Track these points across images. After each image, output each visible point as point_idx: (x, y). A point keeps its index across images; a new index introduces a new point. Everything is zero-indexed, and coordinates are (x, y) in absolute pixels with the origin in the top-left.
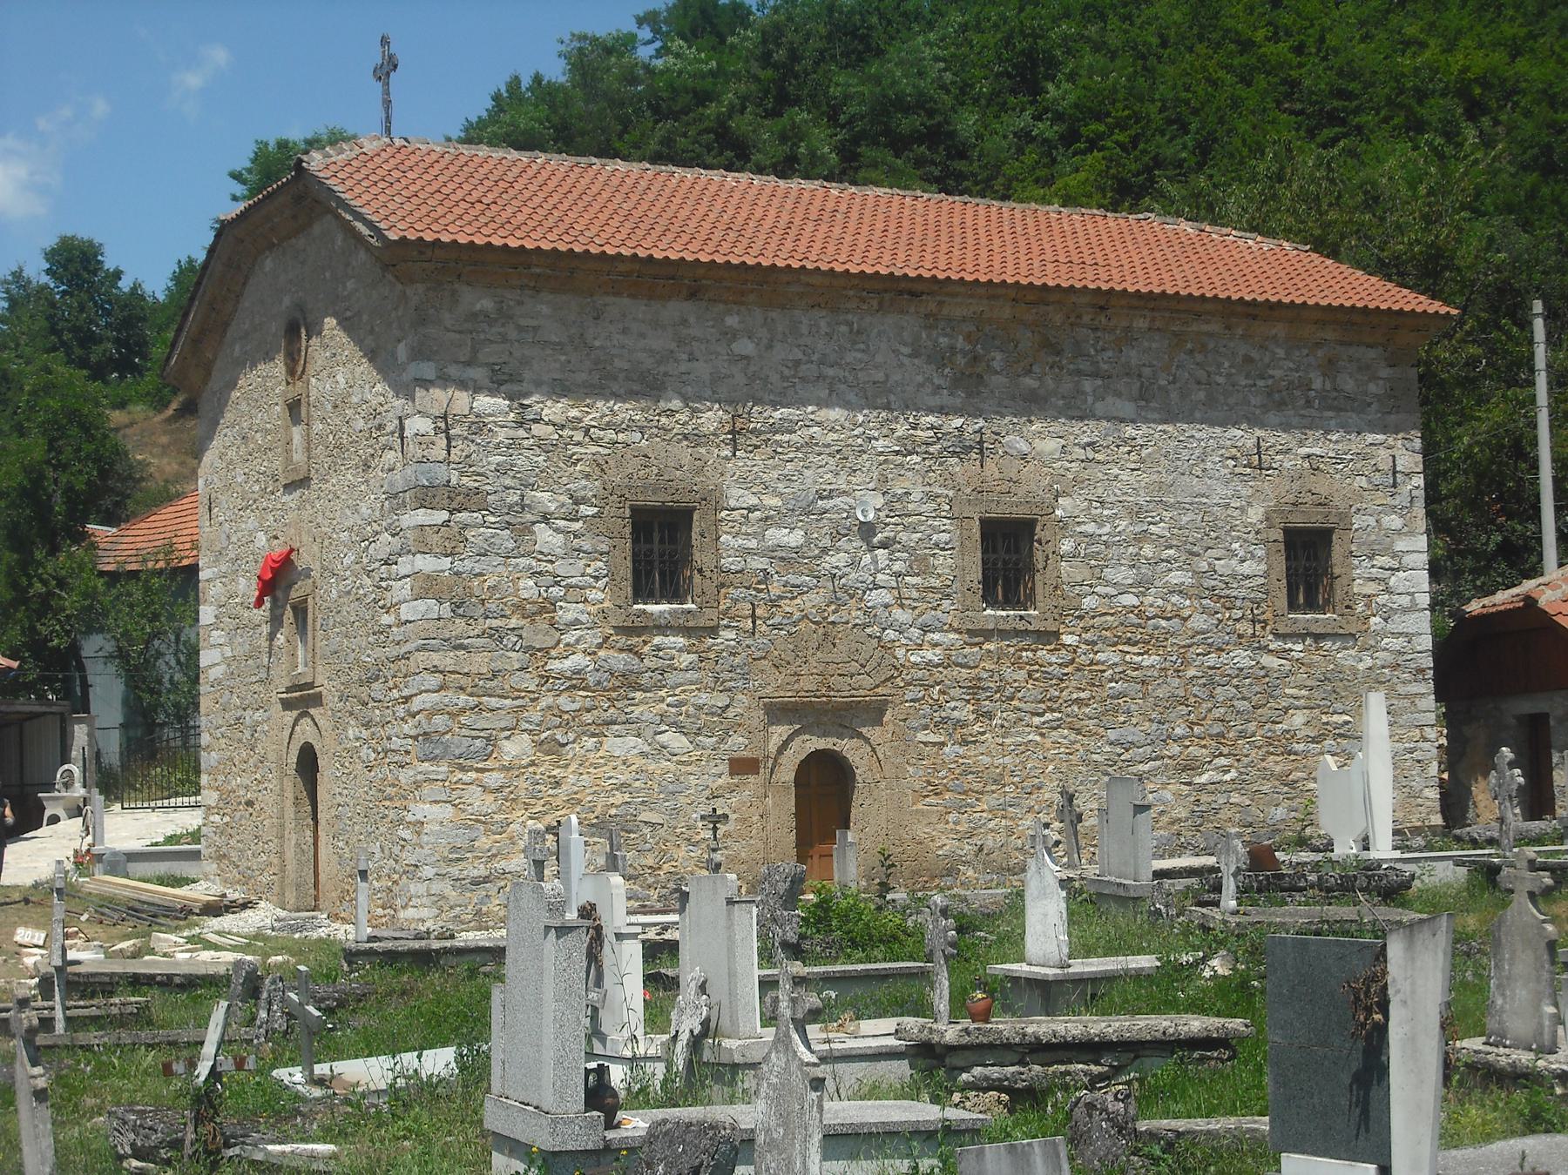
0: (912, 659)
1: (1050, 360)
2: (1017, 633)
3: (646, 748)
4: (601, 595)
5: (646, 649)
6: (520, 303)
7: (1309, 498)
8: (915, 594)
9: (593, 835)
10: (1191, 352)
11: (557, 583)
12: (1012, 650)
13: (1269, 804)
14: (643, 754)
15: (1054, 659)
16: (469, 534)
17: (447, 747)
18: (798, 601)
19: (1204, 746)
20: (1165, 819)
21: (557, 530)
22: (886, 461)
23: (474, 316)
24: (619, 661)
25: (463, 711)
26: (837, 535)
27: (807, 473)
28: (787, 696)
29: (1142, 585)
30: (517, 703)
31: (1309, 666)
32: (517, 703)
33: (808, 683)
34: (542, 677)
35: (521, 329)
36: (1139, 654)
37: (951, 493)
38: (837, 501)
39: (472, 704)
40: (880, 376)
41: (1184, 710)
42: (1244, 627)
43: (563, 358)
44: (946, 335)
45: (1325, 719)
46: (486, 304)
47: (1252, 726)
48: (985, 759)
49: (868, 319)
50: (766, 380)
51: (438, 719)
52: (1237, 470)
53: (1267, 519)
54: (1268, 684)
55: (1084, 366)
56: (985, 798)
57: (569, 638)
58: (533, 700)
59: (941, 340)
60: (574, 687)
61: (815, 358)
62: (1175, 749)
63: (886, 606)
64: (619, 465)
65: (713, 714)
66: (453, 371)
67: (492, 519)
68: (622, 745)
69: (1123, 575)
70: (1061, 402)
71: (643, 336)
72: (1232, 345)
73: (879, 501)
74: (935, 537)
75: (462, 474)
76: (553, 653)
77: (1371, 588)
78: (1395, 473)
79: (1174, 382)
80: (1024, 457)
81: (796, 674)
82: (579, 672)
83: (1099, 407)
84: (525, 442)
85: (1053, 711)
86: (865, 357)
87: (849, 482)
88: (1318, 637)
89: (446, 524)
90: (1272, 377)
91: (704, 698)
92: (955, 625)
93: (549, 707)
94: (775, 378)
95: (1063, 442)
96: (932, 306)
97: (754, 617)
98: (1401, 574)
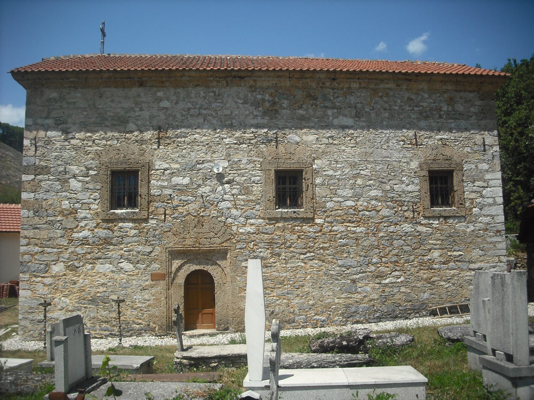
0: (240, 231)
1: (311, 102)
2: (293, 219)
3: (114, 269)
4: (96, 207)
5: (116, 228)
6: (69, 93)
7: (441, 157)
8: (242, 203)
9: (89, 304)
10: (381, 97)
11: (78, 202)
12: (290, 226)
13: (420, 292)
14: (113, 272)
15: (311, 230)
16: (42, 184)
17: (29, 268)
18: (186, 207)
19: (388, 267)
20: (367, 299)
21: (79, 181)
22: (230, 148)
23: (50, 100)
24: (102, 233)
25: (36, 253)
26: (205, 179)
27: (192, 153)
28: (179, 247)
29: (357, 197)
30: (59, 250)
31: (442, 230)
32: (59, 250)
33: (189, 242)
34: (70, 240)
35: (68, 103)
36: (354, 227)
37: (261, 160)
38: (206, 165)
39: (40, 251)
40: (228, 112)
41: (377, 251)
42: (409, 214)
43: (85, 113)
44: (260, 94)
45: (449, 253)
46: (55, 95)
47: (412, 258)
48: (276, 274)
49: (223, 90)
50: (174, 117)
51: (26, 257)
52: (405, 146)
53: (420, 167)
54: (421, 240)
55: (328, 104)
56: (275, 290)
57: (82, 224)
58: (66, 249)
59: (258, 96)
60: (83, 244)
61: (197, 107)
62: (372, 268)
63: (229, 208)
64: (107, 154)
65: (144, 255)
66: (39, 121)
67: (52, 177)
68: (104, 268)
69: (348, 192)
70: (316, 120)
71: (120, 102)
72: (402, 93)
73: (226, 164)
74: (253, 178)
75: (41, 160)
76: (75, 230)
77: (473, 196)
78: (484, 145)
79: (373, 109)
80: (297, 143)
81: (183, 238)
82: (86, 238)
83: (336, 122)
84: (67, 147)
85: (311, 252)
86: (221, 105)
87: (212, 157)
88: (446, 218)
89: (33, 180)
90: (421, 106)
91: (140, 248)
92: (262, 216)
93: (72, 252)
94: (179, 116)
95: (317, 136)
96: (252, 83)
97: (165, 214)
98: (488, 189)
